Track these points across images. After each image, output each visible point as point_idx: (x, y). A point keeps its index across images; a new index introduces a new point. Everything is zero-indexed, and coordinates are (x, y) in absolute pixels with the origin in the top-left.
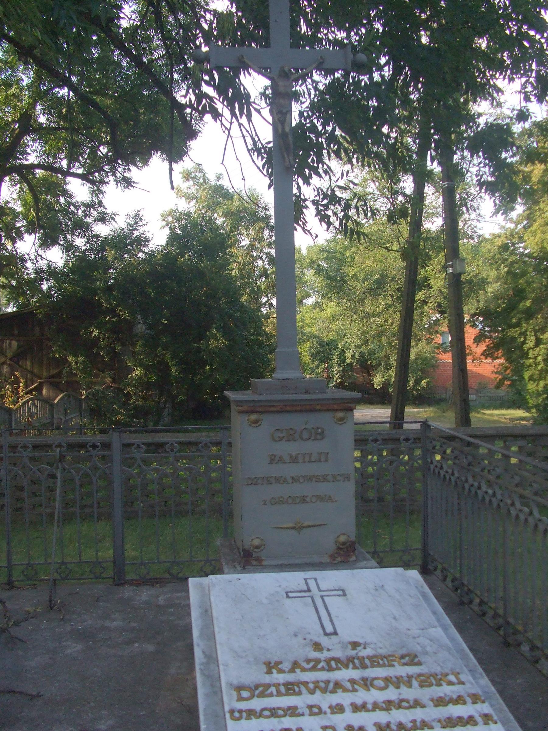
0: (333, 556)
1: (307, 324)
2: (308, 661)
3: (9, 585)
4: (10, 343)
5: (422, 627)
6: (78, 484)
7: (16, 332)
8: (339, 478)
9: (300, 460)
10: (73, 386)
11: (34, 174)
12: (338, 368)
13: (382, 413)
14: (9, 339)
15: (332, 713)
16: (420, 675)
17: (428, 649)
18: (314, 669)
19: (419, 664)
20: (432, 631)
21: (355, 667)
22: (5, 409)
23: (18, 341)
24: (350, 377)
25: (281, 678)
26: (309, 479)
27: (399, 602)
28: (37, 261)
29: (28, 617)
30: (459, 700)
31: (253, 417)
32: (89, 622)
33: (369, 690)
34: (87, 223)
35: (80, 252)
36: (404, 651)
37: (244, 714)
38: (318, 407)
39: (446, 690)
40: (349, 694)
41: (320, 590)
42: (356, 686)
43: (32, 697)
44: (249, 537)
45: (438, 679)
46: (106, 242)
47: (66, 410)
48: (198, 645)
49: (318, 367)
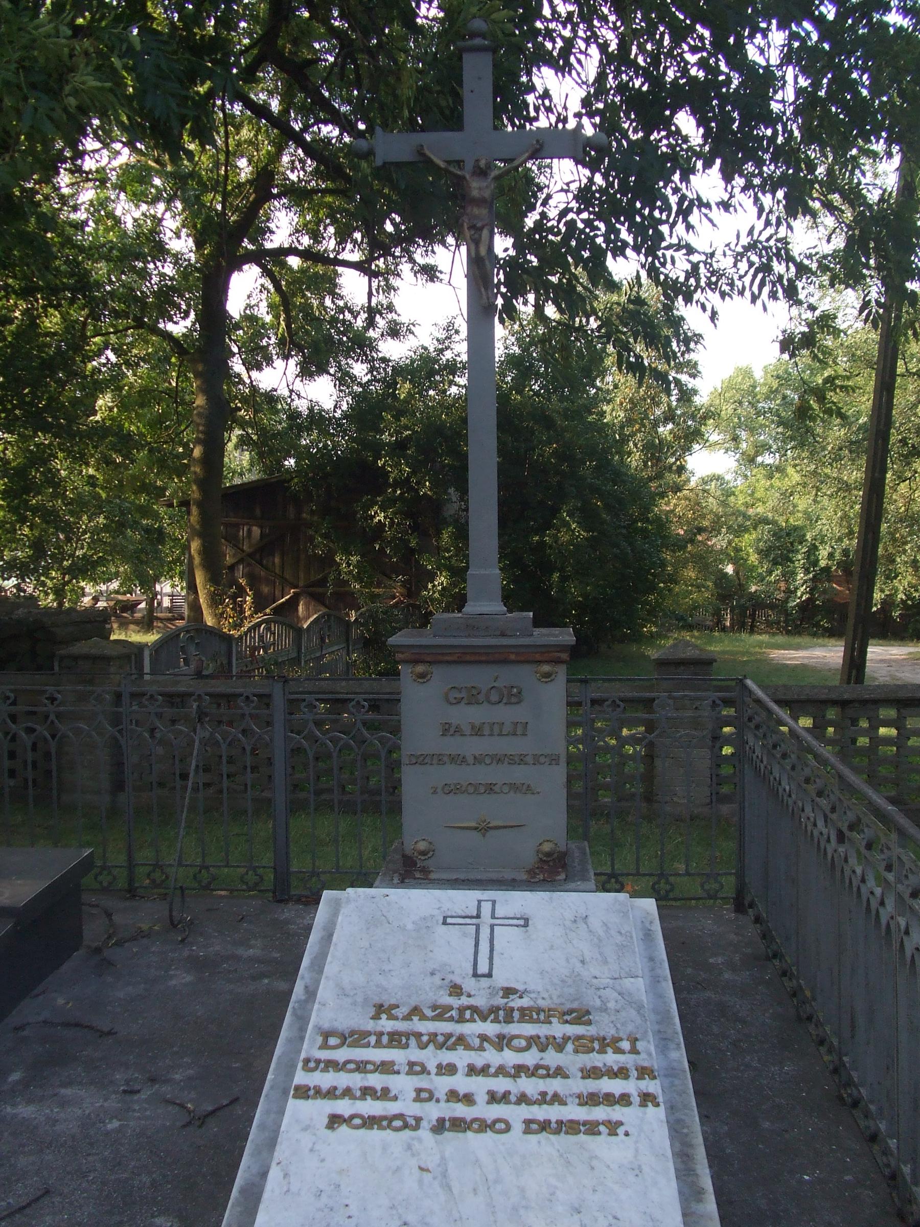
0: (532, 872)
1: (759, 500)
2: (434, 1007)
3: (129, 891)
4: (249, 531)
5: (617, 976)
6: (311, 757)
7: (258, 512)
8: (542, 760)
9: (487, 732)
10: (345, 599)
11: (284, 265)
12: (805, 575)
13: (829, 654)
14: (247, 524)
15: (437, 1074)
16: (579, 1038)
17: (611, 1005)
18: (439, 1017)
19: (589, 1023)
20: (628, 983)
21: (496, 1021)
22: (220, 636)
23: (261, 527)
24: (825, 592)
25: (386, 1025)
26: (499, 759)
27: (600, 940)
28: (293, 400)
29: (140, 935)
30: (621, 1073)
31: (420, 668)
32: (217, 948)
33: (501, 1050)
34: (370, 338)
35: (360, 384)
36: (575, 1005)
37: (322, 1065)
38: (513, 657)
39: (611, 1059)
40: (473, 1053)
41: (493, 917)
42: (485, 1044)
43: (103, 1034)
44: (414, 837)
45: (605, 1044)
46: (400, 371)
47: (322, 640)
48: (303, 978)
49: (770, 572)
